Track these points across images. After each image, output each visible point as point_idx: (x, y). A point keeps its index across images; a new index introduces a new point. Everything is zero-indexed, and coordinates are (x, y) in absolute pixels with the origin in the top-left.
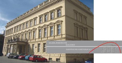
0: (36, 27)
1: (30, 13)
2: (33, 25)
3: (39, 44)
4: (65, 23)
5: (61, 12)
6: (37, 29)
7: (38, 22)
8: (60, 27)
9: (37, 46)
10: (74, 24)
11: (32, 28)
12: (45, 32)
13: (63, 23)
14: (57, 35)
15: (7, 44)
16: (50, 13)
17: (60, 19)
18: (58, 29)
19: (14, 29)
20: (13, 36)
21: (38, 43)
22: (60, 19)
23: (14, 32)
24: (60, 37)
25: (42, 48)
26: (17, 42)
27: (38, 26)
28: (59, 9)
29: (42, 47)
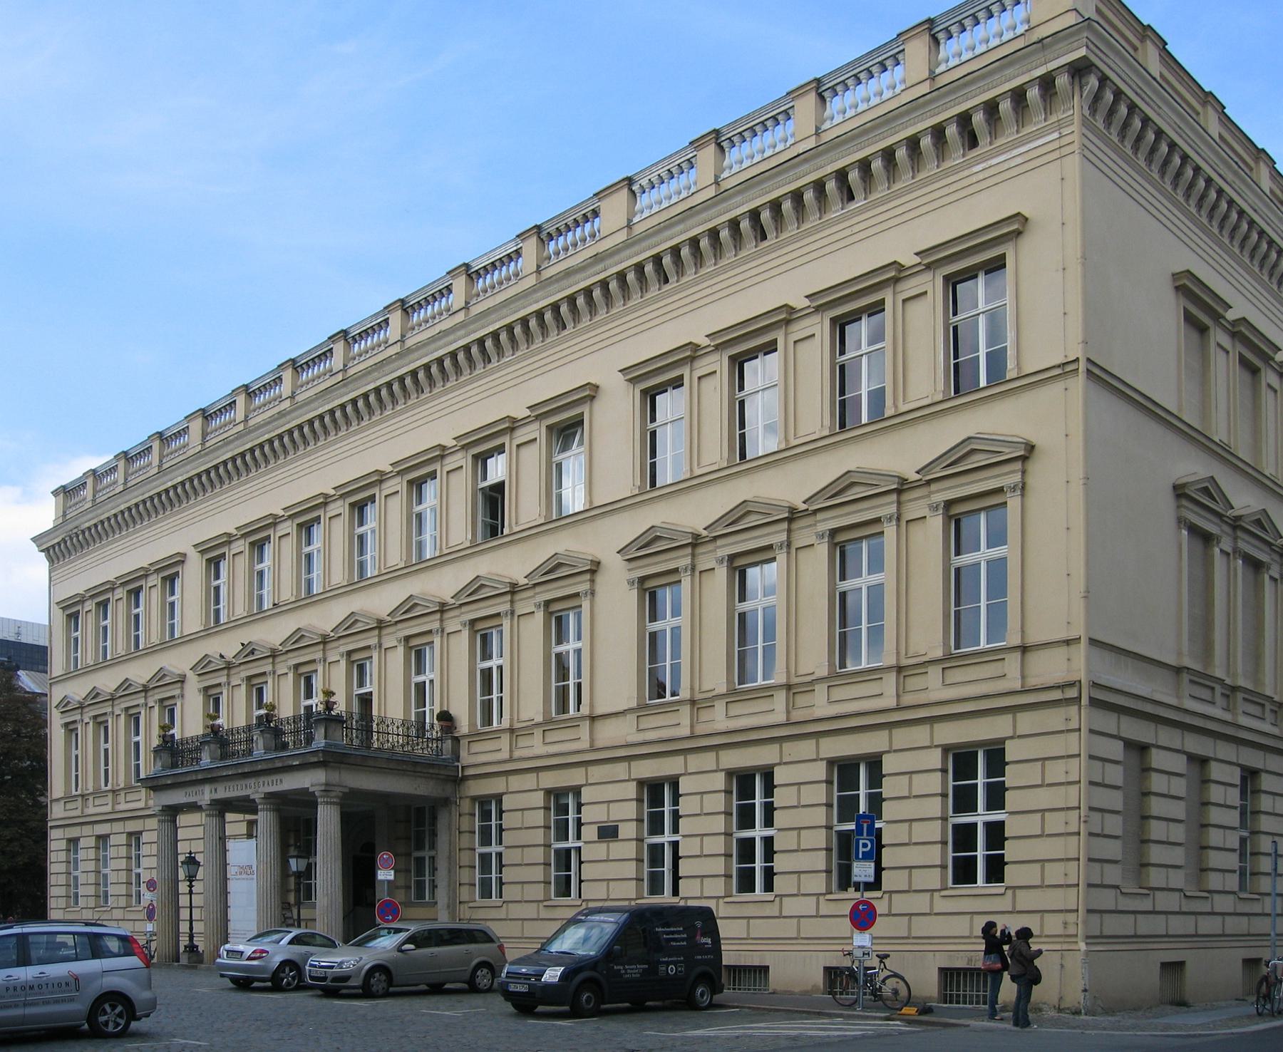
0: (180, 661)
1: (239, 436)
2: (339, 576)
3: (655, 792)
4: (1078, 473)
5: (1009, 300)
6: (192, 679)
7: (191, 618)
8: (997, 538)
9: (630, 810)
10: (1180, 492)
11: (81, 680)
12: (561, 660)
13: (1039, 471)
14: (838, 675)
15: (155, 789)
16: (820, 327)
17: (998, 420)
18: (487, 674)
19: (194, 572)
20: (192, 679)
21: (649, 769)
22: (998, 420)
23: (215, 625)
24: (499, 756)
25: (718, 845)
26: (331, 759)
27: (630, 527)
28: (974, 261)
29: (719, 824)
